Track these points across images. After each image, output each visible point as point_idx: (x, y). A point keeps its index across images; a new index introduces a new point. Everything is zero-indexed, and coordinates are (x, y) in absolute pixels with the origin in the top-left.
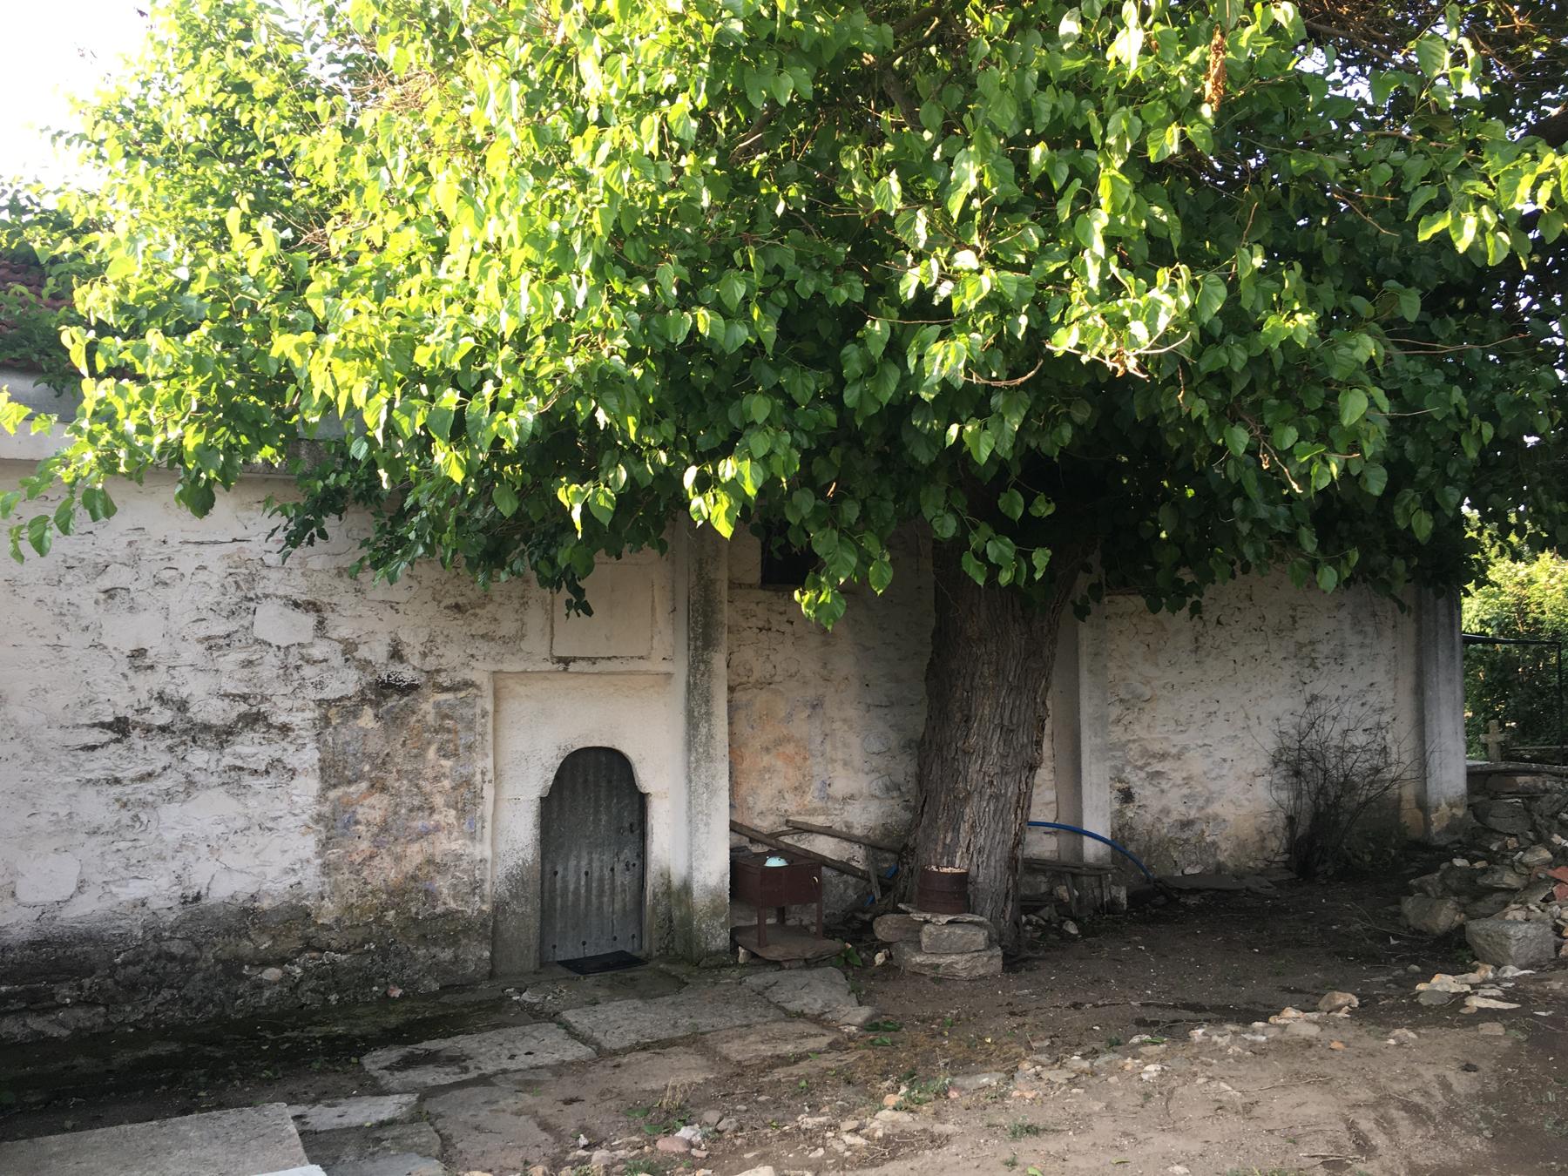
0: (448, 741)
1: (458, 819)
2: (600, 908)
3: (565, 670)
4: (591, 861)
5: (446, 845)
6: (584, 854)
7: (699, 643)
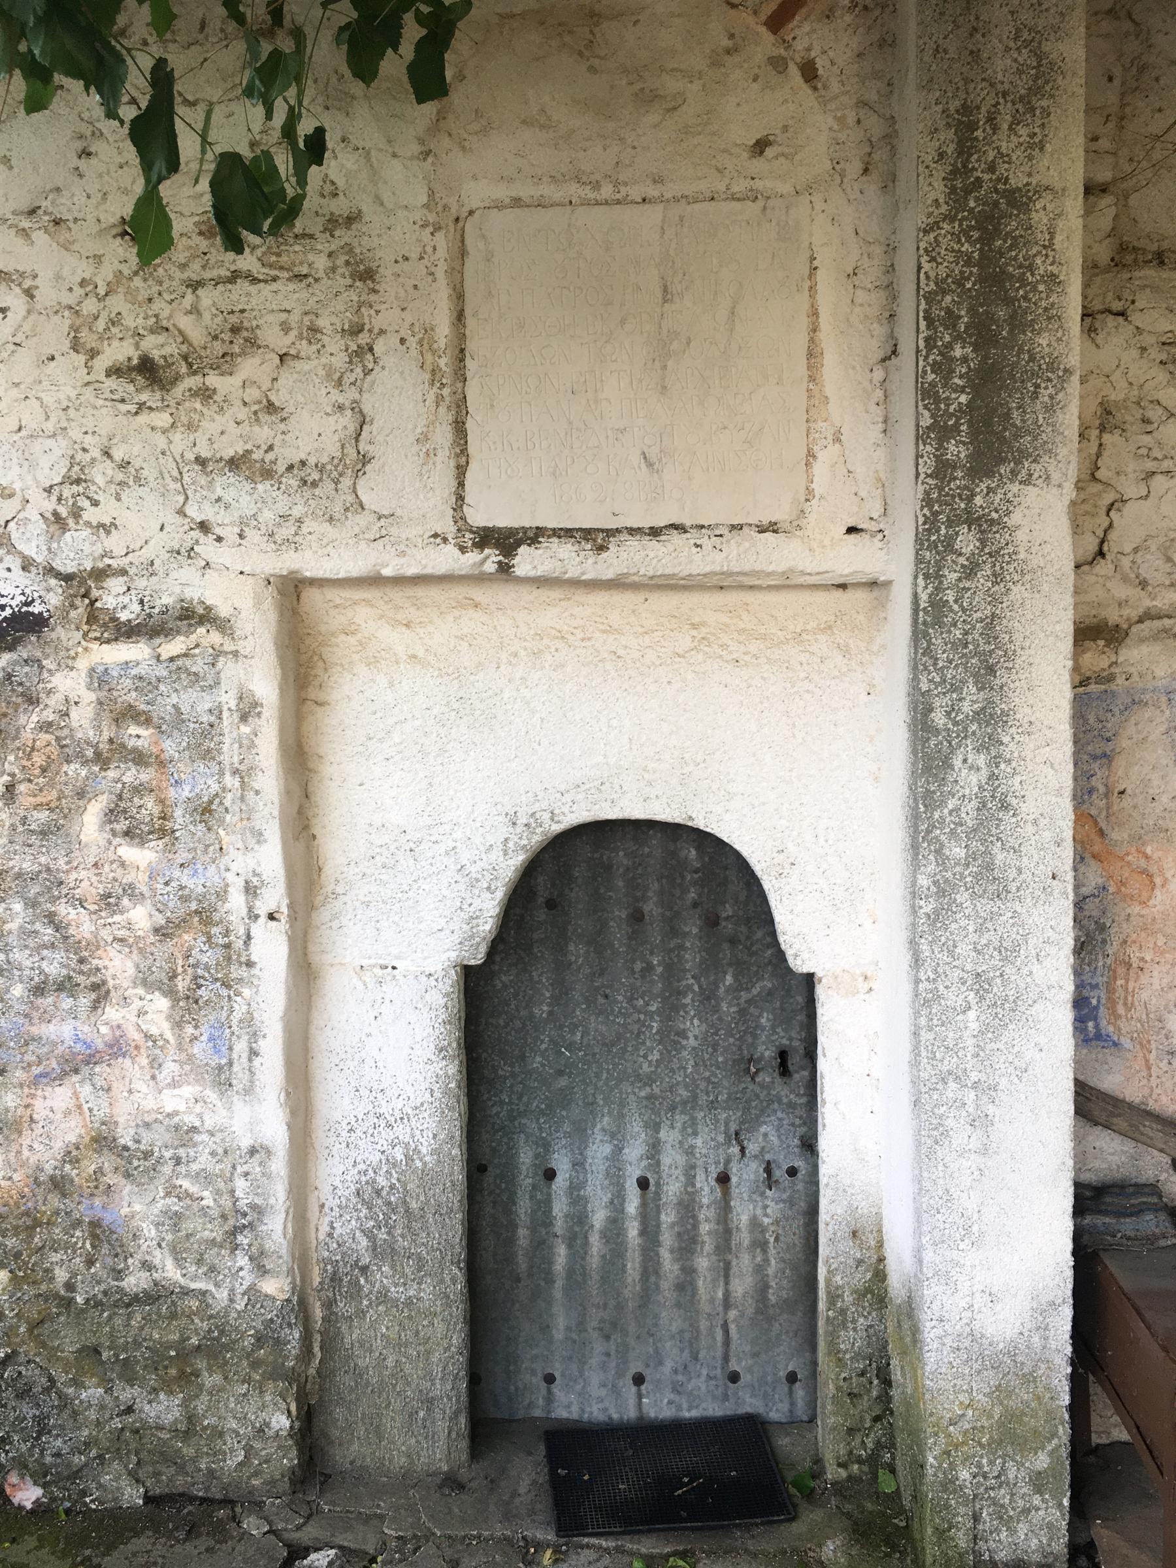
0: (138, 790)
1: (178, 1025)
2: (686, 1285)
3: (504, 569)
4: (654, 1150)
5: (142, 1098)
6: (636, 1126)
7: (956, 450)
